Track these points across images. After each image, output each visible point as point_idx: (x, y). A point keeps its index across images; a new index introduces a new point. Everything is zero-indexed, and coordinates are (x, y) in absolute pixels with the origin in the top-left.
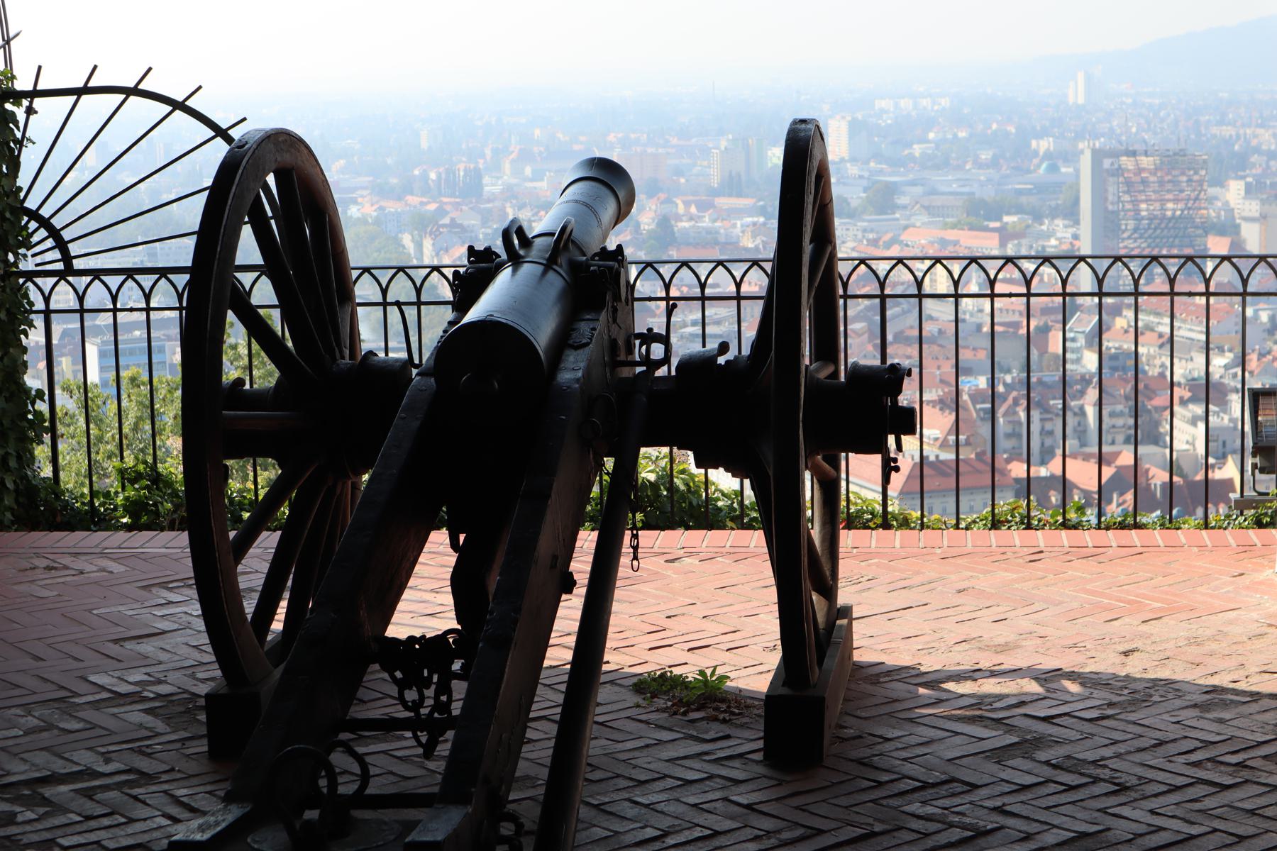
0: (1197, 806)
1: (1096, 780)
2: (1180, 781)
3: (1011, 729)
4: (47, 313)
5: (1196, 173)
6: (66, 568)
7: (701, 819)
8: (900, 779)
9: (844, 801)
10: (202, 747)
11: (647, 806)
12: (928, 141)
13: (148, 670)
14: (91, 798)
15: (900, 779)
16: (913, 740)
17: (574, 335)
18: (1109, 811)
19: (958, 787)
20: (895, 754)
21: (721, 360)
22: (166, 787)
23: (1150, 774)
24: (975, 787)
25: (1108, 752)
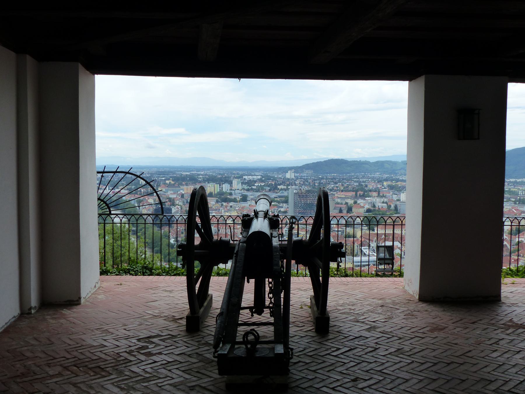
1: (393, 336)
3: (367, 324)
4: (185, 224)
5: (314, 194)
8: (349, 336)
12: (255, 186)
13: (160, 309)
14: (164, 341)
15: (349, 336)
16: (347, 327)
18: (401, 343)
24: (367, 338)
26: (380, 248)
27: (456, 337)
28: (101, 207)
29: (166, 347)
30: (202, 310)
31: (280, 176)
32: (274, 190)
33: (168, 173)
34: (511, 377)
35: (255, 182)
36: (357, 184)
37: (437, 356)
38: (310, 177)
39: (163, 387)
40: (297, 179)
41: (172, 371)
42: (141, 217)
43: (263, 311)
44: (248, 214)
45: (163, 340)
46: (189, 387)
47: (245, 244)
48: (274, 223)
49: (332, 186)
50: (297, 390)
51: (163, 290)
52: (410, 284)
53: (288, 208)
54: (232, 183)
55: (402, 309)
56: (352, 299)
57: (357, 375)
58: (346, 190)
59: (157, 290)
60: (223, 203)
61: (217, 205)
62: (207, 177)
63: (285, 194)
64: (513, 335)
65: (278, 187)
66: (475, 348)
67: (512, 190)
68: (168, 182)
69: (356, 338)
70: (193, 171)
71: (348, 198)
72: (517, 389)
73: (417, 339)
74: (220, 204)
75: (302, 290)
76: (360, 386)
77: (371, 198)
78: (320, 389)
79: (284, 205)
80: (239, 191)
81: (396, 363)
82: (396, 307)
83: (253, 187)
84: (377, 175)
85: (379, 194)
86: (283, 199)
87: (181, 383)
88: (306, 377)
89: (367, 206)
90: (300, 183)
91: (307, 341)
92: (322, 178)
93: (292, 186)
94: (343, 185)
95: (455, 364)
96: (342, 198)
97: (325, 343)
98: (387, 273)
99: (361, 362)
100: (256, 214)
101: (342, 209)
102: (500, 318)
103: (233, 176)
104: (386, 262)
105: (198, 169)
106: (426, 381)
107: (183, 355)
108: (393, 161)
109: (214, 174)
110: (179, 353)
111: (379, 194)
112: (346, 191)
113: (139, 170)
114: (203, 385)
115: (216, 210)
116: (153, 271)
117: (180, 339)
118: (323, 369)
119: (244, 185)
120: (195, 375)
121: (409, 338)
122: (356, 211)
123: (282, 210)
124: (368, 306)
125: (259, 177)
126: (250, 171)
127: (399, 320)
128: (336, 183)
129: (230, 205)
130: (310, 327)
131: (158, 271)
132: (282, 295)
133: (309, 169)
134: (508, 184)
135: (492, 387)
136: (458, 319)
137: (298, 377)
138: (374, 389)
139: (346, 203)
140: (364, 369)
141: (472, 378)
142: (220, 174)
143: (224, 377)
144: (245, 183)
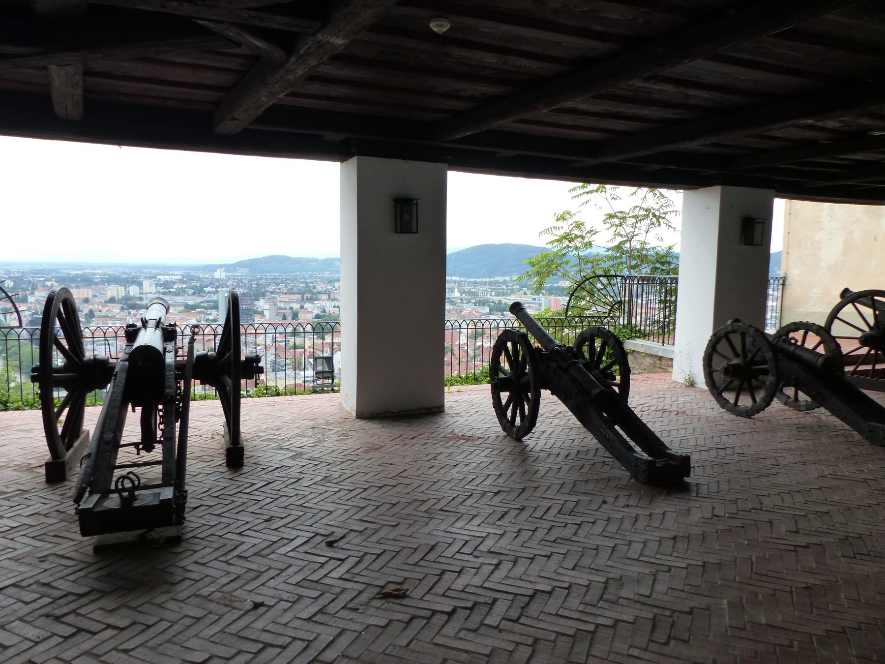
0: (351, 466)
1: (322, 462)
3: (292, 451)
7: (219, 484)
11: (200, 482)
13: (8, 457)
14: (8, 500)
26: (318, 360)
27: (392, 456)
29: (11, 507)
30: (71, 451)
31: (207, 276)
32: (199, 293)
33: (49, 271)
34: (444, 494)
35: (174, 283)
36: (304, 285)
37: (369, 480)
40: (229, 279)
41: (16, 539)
42: (12, 331)
43: (154, 447)
44: (133, 324)
46: (39, 558)
47: (127, 363)
48: (169, 334)
49: (274, 287)
50: (193, 542)
51: (17, 430)
52: (347, 400)
53: (218, 315)
55: (336, 429)
56: (278, 423)
57: (272, 514)
58: (290, 292)
59: (8, 431)
60: (131, 310)
61: (123, 313)
63: (214, 297)
64: (453, 448)
65: (205, 289)
66: (411, 466)
67: (472, 290)
68: (48, 284)
69: (277, 468)
70: (86, 269)
71: (293, 302)
72: (449, 506)
73: (349, 463)
74: (126, 311)
75: (215, 416)
76: (274, 526)
77: (321, 302)
79: (213, 311)
81: (321, 494)
82: (329, 428)
83: (171, 290)
84: (327, 274)
85: (329, 297)
86: (212, 304)
87: (28, 555)
88: (207, 523)
89: (316, 312)
90: (233, 285)
92: (261, 279)
94: (286, 287)
95: (387, 487)
96: (286, 302)
97: (237, 479)
98: (326, 389)
100: (145, 323)
101: (286, 315)
102: (441, 430)
103: (144, 275)
104: (325, 375)
106: (353, 511)
108: (293, 257)
109: (117, 274)
110: (30, 513)
111: (329, 297)
112: (290, 294)
113: (4, 267)
114: (60, 553)
115: (121, 319)
116: (8, 405)
117: (35, 494)
118: (231, 511)
120: (51, 541)
121: (340, 463)
122: (302, 317)
123: (211, 317)
124: (296, 429)
125: (179, 277)
126: (167, 269)
127: (331, 443)
128: (278, 284)
129: (141, 313)
130: (222, 460)
131: (16, 405)
132: (178, 424)
134: (468, 285)
135: (424, 507)
136: (398, 435)
137: (196, 526)
139: (291, 308)
140: (282, 505)
141: (404, 500)
142: (125, 273)
143: (94, 538)
144: (161, 285)
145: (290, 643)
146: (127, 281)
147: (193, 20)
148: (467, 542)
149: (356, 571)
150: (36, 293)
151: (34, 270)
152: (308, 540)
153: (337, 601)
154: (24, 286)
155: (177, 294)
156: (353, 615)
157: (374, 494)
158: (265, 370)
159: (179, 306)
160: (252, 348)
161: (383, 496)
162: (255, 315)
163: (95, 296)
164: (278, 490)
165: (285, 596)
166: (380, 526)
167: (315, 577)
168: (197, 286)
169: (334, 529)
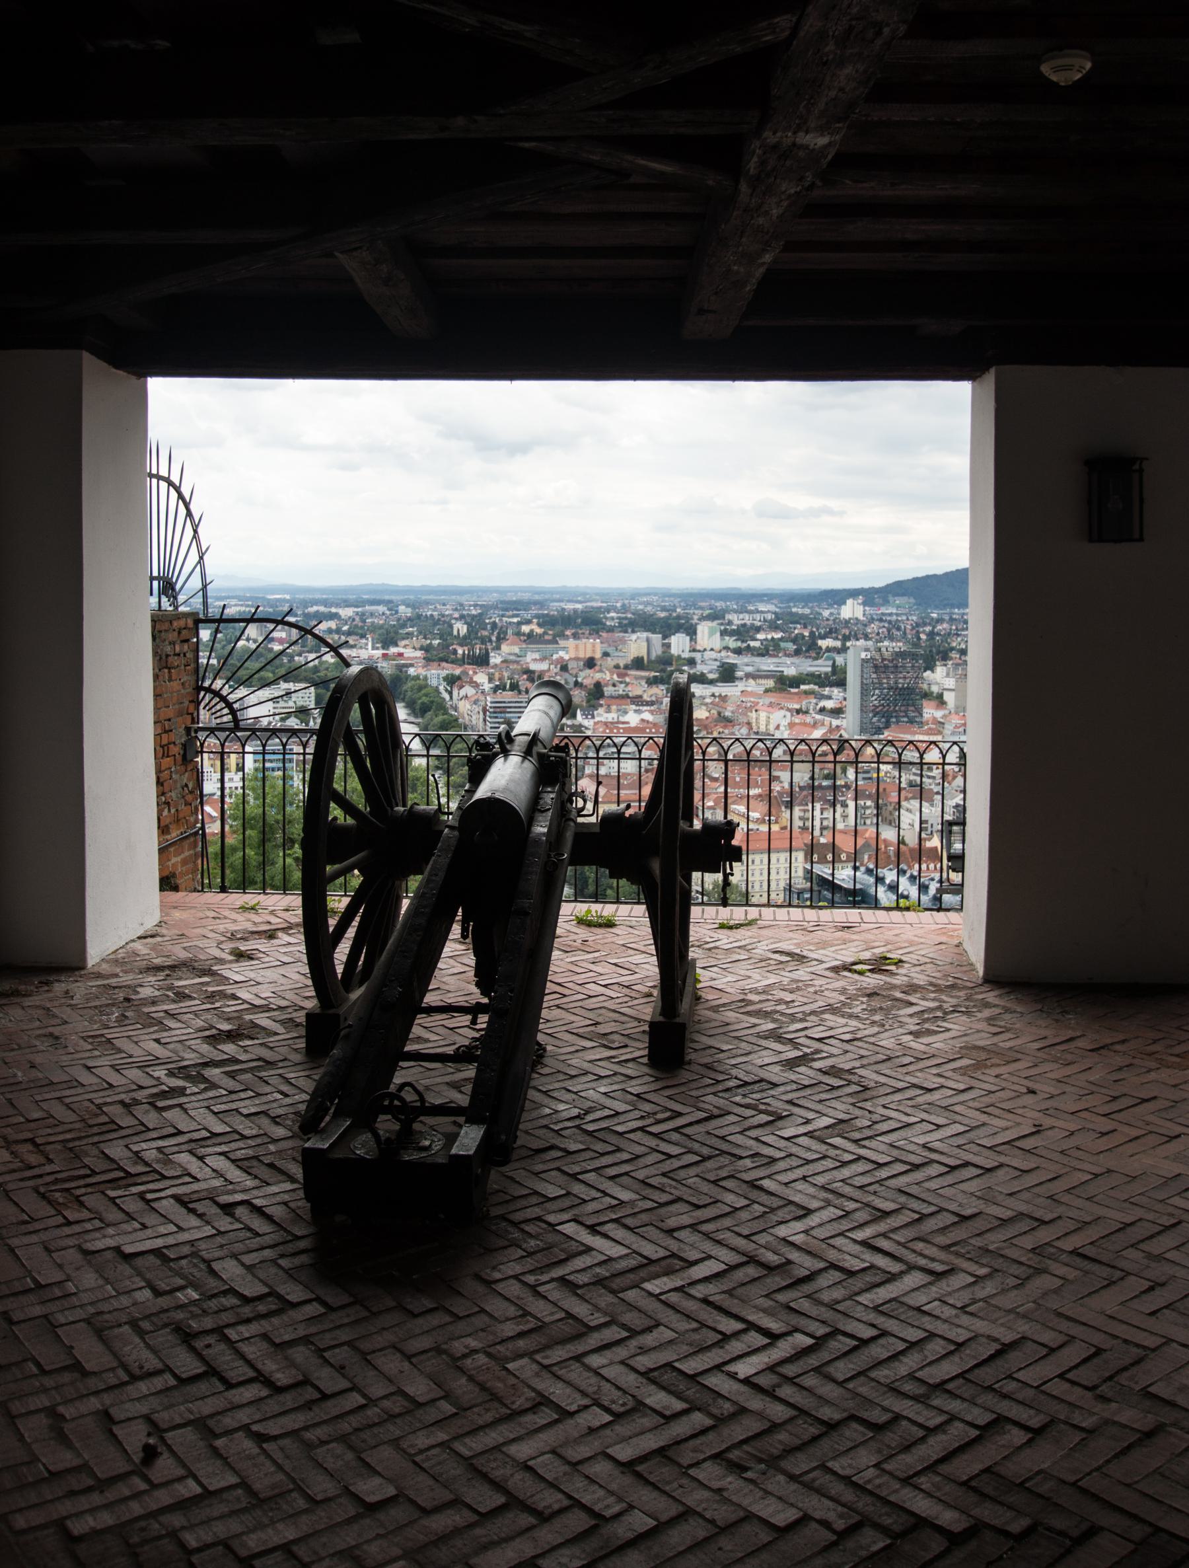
1: (850, 1083)
2: (900, 1085)
6: (225, 918)
7: (608, 1102)
9: (694, 1093)
10: (301, 1044)
14: (233, 1078)
16: (740, 1052)
17: (542, 802)
19: (764, 1085)
20: (727, 1061)
21: (627, 814)
22: (280, 1071)
23: (883, 1079)
24: (775, 1085)
25: (857, 1064)
28: (213, 710)
38: (904, 618)
39: (154, 1205)
40: (872, 620)
45: (231, 1075)
54: (695, 633)
62: (629, 616)
68: (525, 629)
78: (557, 1228)
80: (713, 655)
83: (752, 644)
90: (878, 634)
91: (603, 1090)
92: (940, 621)
93: (857, 640)
99: (717, 1155)
105: (604, 595)
106: (862, 1216)
107: (262, 1115)
109: (649, 608)
115: (651, 703)
119: (727, 638)
123: (829, 704)
126: (745, 599)
130: (640, 1049)
133: (903, 595)
138: (704, 1234)
142: (664, 609)
144: (731, 633)
145: (561, 1511)
146: (668, 626)
147: (521, 144)
148: (1099, 1352)
149: (790, 1370)
150: (505, 648)
151: (502, 602)
152: (725, 1271)
153: (711, 1436)
154: (485, 633)
155: (763, 652)
156: (731, 1482)
157: (930, 1181)
158: (744, 857)
159: (767, 677)
160: (915, 774)
161: (947, 1192)
162: (925, 703)
163: (606, 654)
164: (1009, 1111)
165: (609, 1395)
166: (904, 1267)
167: (690, 1366)
168: (804, 637)
169: (794, 1256)
